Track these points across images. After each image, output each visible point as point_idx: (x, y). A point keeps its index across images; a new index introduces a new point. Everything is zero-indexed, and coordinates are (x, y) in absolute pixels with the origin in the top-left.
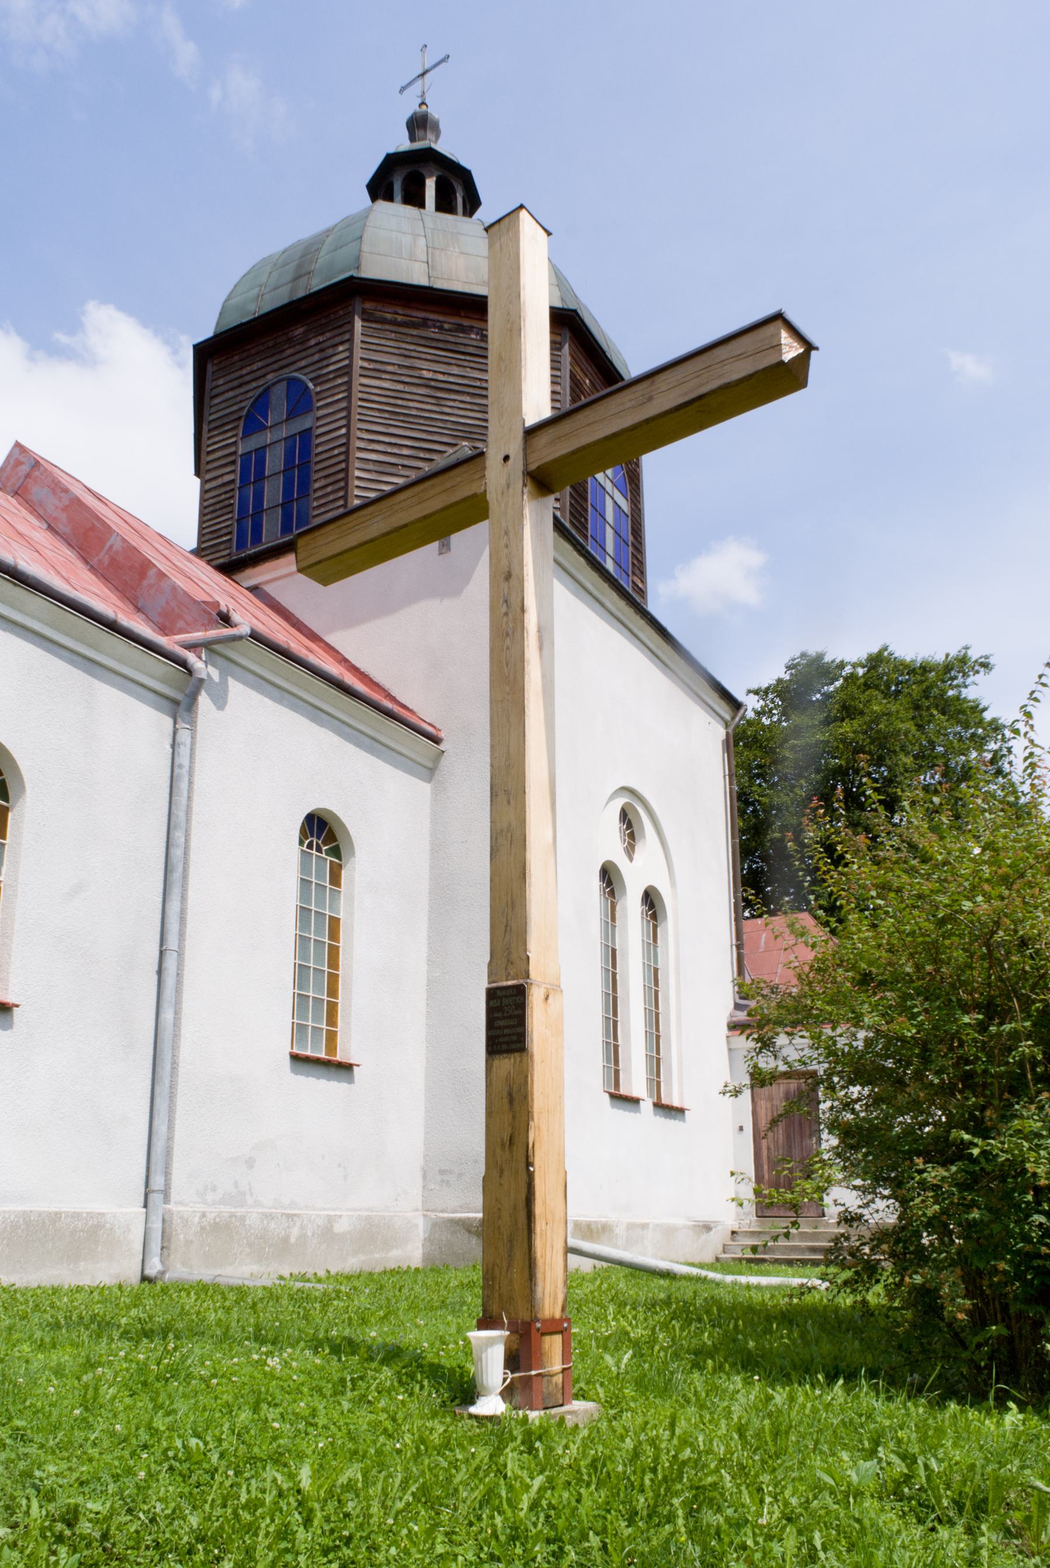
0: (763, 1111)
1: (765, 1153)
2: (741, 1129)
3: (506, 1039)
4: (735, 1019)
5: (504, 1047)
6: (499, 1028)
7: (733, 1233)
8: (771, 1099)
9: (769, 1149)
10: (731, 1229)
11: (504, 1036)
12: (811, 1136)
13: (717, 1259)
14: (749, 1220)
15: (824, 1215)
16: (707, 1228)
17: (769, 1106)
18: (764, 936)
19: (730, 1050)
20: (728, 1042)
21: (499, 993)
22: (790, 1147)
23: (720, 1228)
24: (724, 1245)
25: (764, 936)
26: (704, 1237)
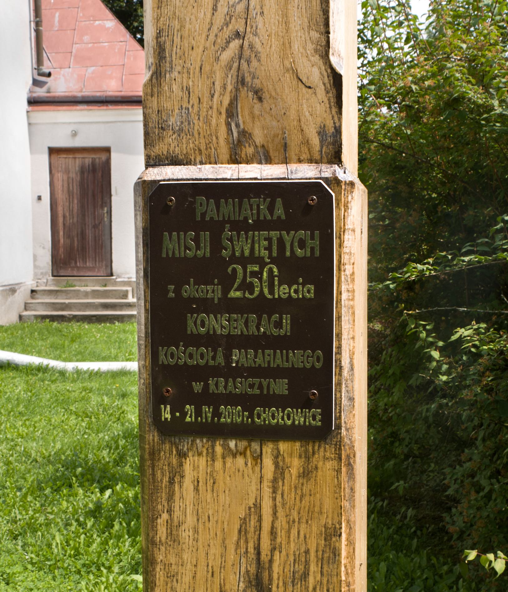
0: (60, 183)
1: (61, 220)
2: (39, 198)
3: (240, 386)
4: (35, 95)
5: (231, 415)
6: (211, 340)
7: (33, 291)
8: (67, 171)
9: (64, 217)
10: (30, 288)
11: (230, 372)
12: (102, 207)
13: (20, 317)
14: (47, 282)
15: (112, 275)
16: (12, 290)
17: (65, 178)
18: (57, 15)
19: (29, 124)
20: (28, 117)
21: (206, 208)
22: (84, 216)
23: (22, 289)
24: (26, 303)
25: (57, 15)
26: (10, 299)
